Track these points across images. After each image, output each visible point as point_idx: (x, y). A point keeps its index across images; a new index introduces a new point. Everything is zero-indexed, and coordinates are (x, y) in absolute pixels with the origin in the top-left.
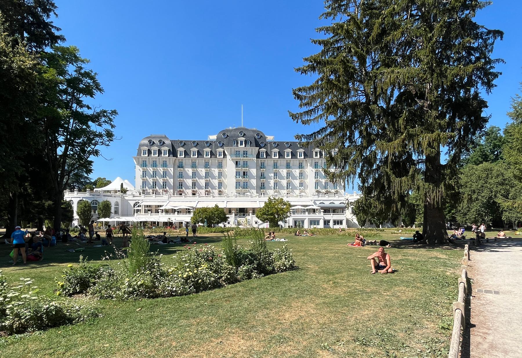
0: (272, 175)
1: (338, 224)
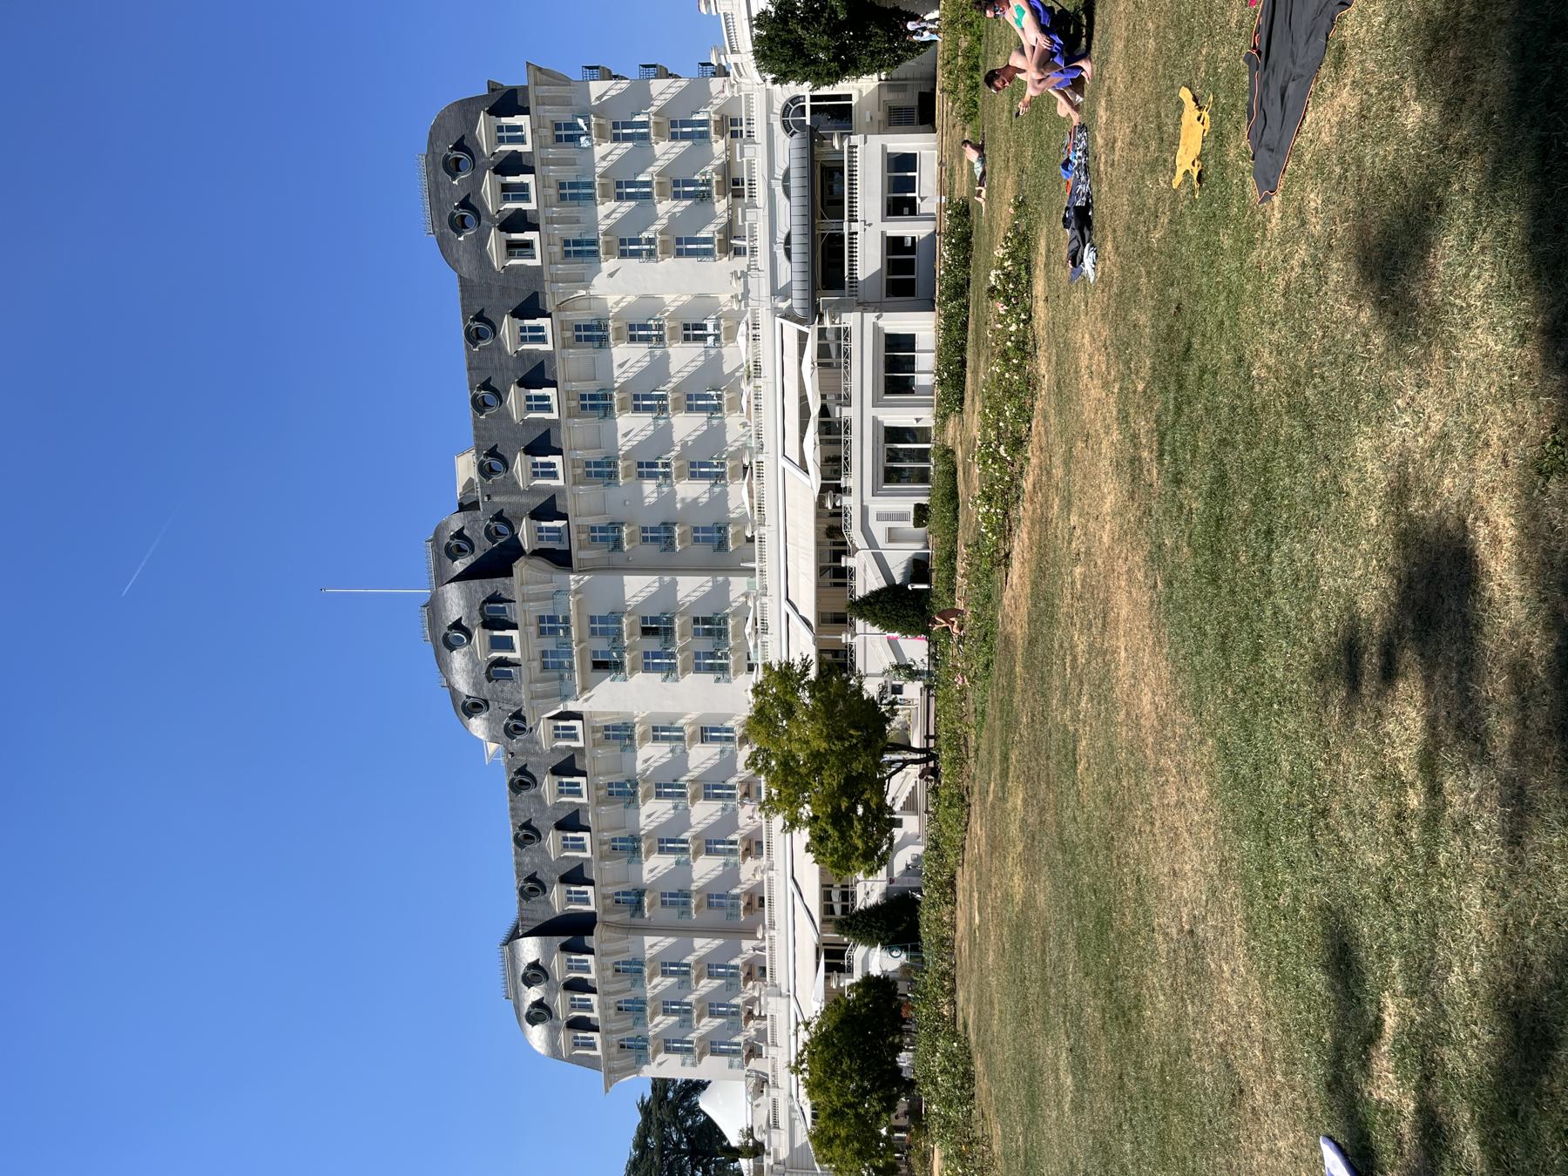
0: (649, 487)
1: (910, 184)
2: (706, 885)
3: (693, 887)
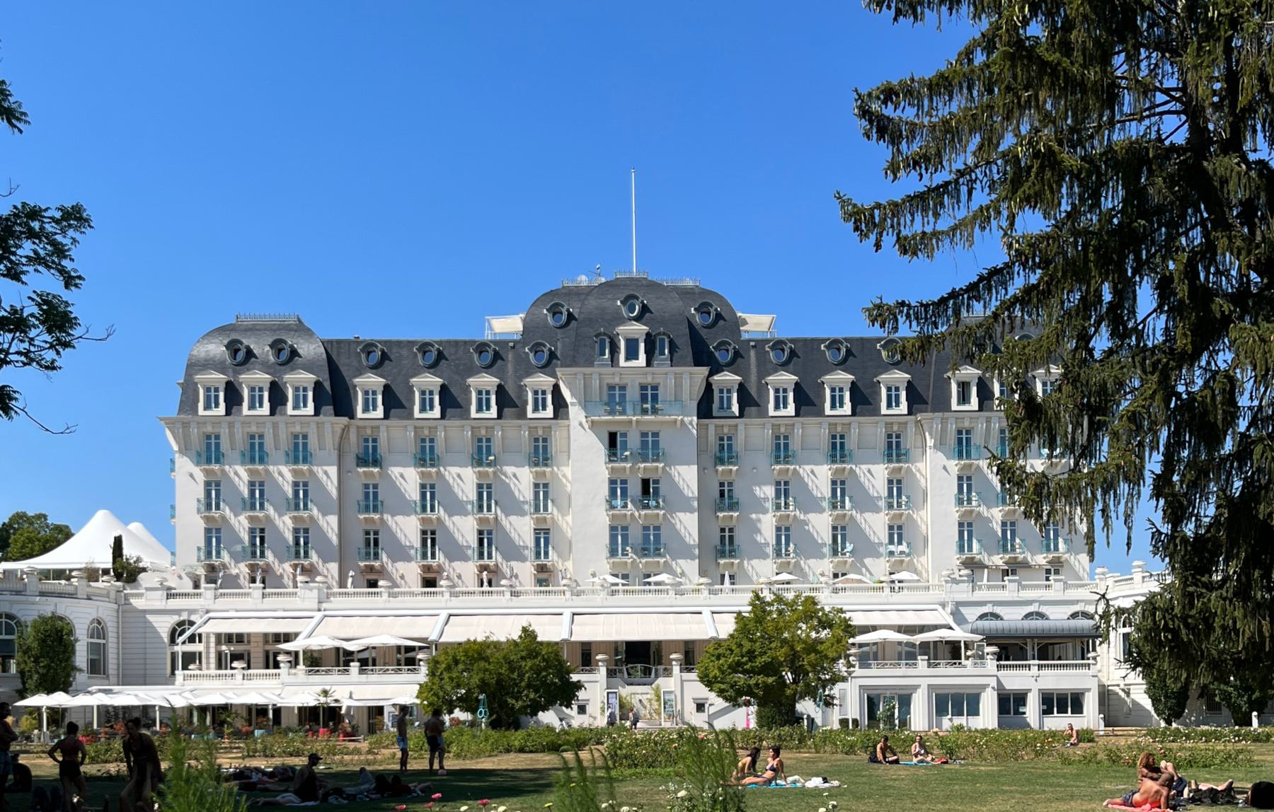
0: (769, 491)
1: (1062, 710)
2: (503, 528)
3: (387, 517)
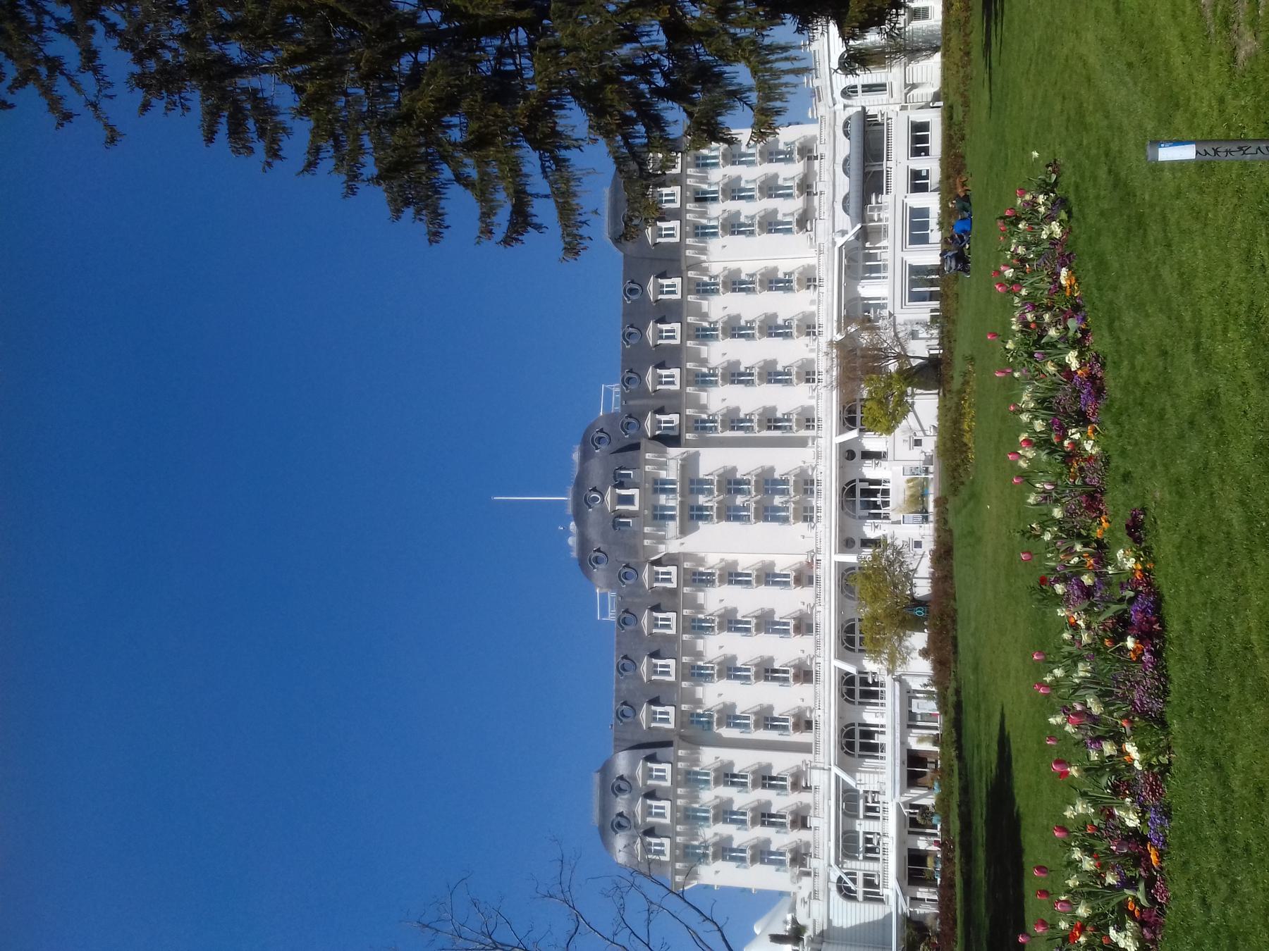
1: (925, 139)
